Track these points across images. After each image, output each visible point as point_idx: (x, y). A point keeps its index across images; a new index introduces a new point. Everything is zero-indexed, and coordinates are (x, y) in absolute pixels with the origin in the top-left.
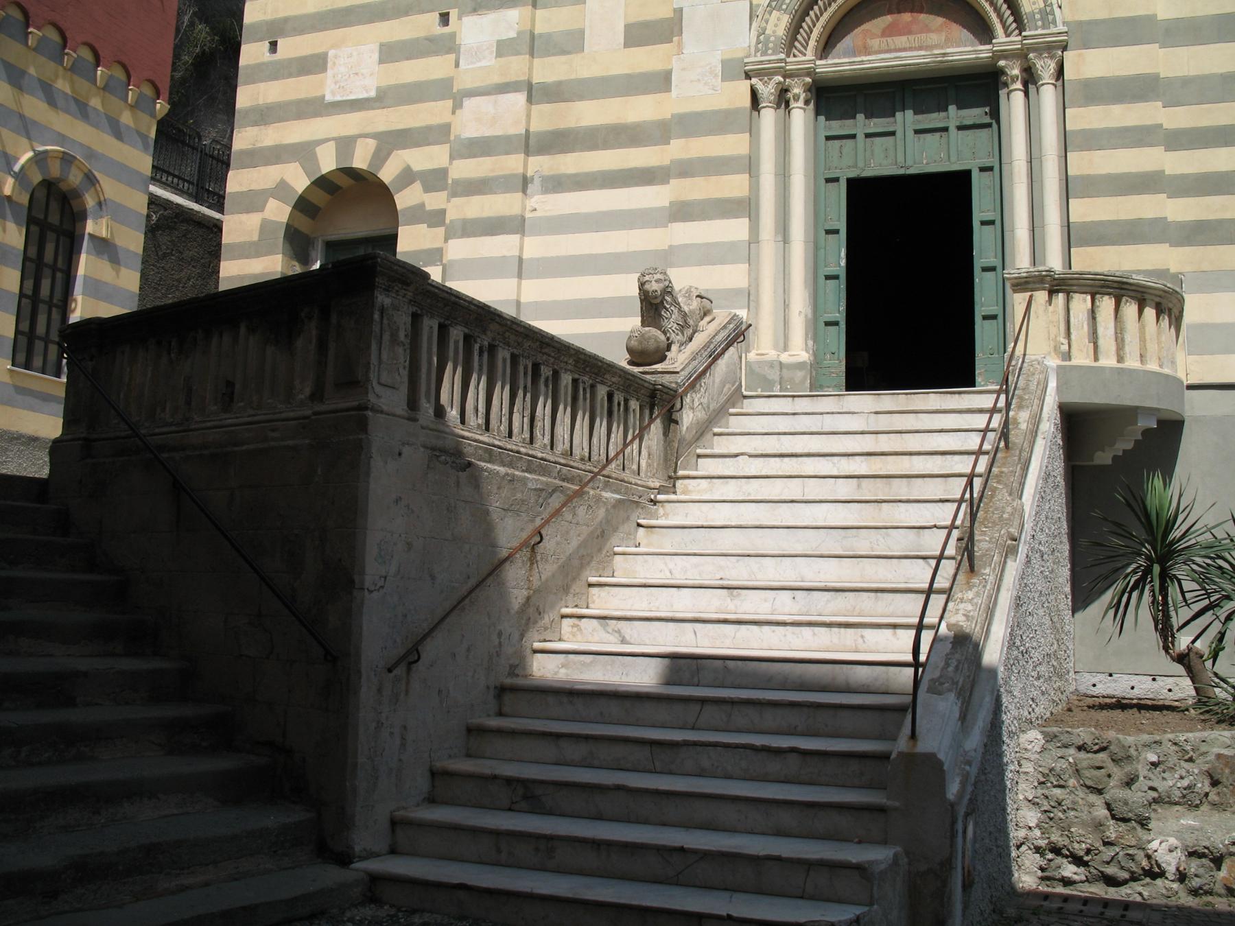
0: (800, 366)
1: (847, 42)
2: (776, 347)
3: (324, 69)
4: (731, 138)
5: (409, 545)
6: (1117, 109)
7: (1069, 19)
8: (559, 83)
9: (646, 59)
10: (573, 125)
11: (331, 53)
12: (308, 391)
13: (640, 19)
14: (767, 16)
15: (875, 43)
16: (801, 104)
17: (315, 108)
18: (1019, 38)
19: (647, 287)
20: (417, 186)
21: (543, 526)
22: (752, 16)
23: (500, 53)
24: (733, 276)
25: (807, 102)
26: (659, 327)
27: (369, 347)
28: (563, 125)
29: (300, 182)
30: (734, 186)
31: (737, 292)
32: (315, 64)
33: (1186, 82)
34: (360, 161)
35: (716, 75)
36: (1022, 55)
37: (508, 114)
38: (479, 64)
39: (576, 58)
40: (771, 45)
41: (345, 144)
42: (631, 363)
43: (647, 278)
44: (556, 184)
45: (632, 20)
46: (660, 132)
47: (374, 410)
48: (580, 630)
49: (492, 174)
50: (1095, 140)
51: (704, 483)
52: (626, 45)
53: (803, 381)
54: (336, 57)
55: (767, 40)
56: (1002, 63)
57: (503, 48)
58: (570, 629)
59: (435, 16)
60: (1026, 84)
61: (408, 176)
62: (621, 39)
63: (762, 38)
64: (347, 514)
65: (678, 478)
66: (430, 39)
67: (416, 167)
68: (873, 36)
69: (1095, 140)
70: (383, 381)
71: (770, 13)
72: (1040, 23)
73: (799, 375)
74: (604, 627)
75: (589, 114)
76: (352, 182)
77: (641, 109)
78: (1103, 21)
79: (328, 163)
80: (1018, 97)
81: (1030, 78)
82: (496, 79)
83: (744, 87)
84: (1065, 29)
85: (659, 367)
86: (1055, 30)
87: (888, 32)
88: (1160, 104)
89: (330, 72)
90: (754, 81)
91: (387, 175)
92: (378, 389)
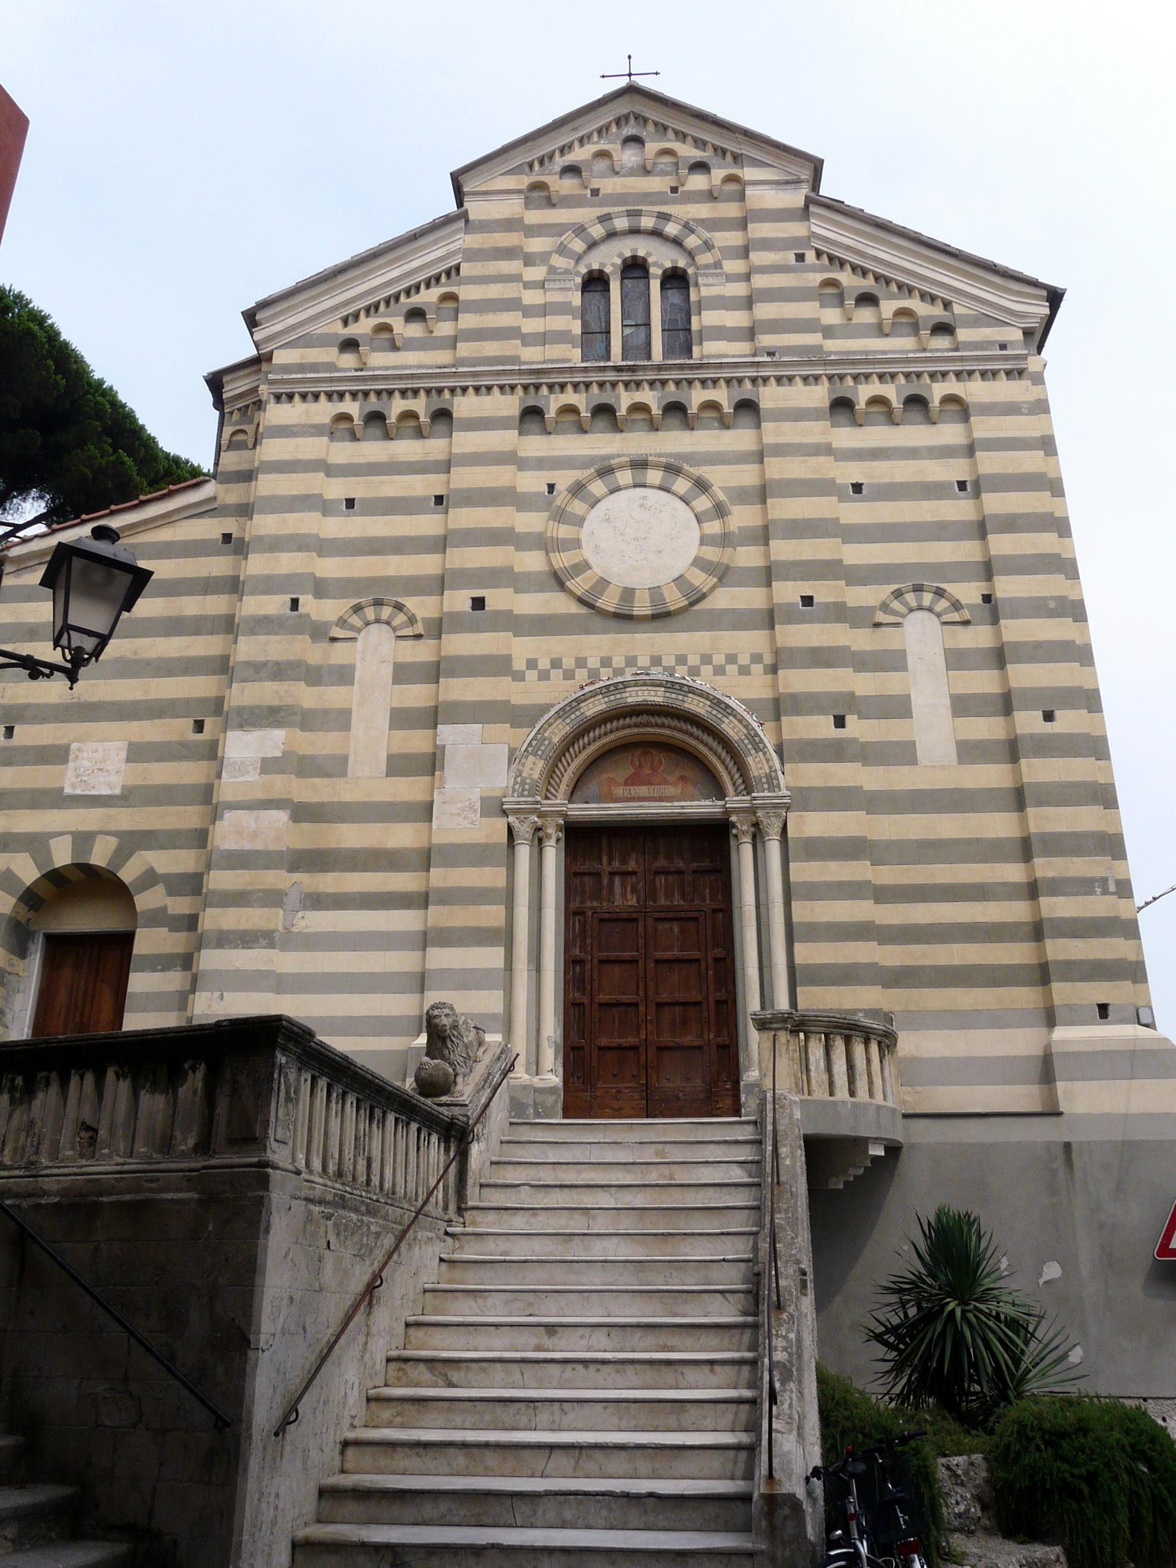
0: (552, 1090)
1: (592, 787)
2: (527, 1072)
3: (65, 761)
4: (488, 870)
5: (291, 1299)
6: (833, 865)
7: (792, 784)
8: (322, 804)
9: (409, 789)
10: (334, 846)
11: (74, 746)
12: (191, 1142)
13: (403, 751)
14: (524, 760)
15: (619, 791)
16: (553, 842)
17: (56, 799)
18: (748, 798)
19: (437, 1021)
20: (160, 889)
21: (381, 1270)
22: (511, 760)
23: (264, 771)
24: (489, 1002)
25: (558, 840)
26: (443, 1058)
27: (269, 1105)
28: (323, 845)
29: (28, 873)
30: (491, 915)
31: (493, 1017)
32: (57, 755)
33: (890, 844)
34: (99, 857)
35: (475, 811)
36: (752, 810)
37: (272, 829)
38: (241, 779)
39: (340, 783)
40: (527, 787)
41: (83, 840)
42: (420, 1094)
43: (436, 1012)
44: (317, 901)
45: (395, 750)
46: (426, 859)
47: (276, 1168)
48: (406, 1374)
49: (250, 888)
50: (815, 891)
51: (492, 1216)
52: (388, 774)
53: (554, 1106)
54: (79, 750)
55: (523, 783)
56: (733, 818)
57: (268, 766)
58: (395, 1374)
59: (189, 723)
60: (754, 837)
61: (150, 878)
62: (383, 767)
63: (519, 779)
64: (246, 1272)
65: (466, 1209)
66: (184, 745)
67: (161, 869)
68: (618, 784)
69: (815, 891)
70: (278, 1137)
71: (527, 757)
72: (766, 786)
73: (550, 1099)
74: (431, 1370)
75: (351, 836)
76: (83, 876)
77: (402, 836)
78: (819, 789)
79: (62, 856)
80: (747, 851)
81: (758, 836)
82: (260, 795)
83: (500, 824)
84: (789, 793)
85: (444, 1099)
86: (780, 794)
87: (631, 781)
88: (869, 863)
89: (71, 765)
90: (511, 819)
91: (128, 874)
92: (274, 1145)
